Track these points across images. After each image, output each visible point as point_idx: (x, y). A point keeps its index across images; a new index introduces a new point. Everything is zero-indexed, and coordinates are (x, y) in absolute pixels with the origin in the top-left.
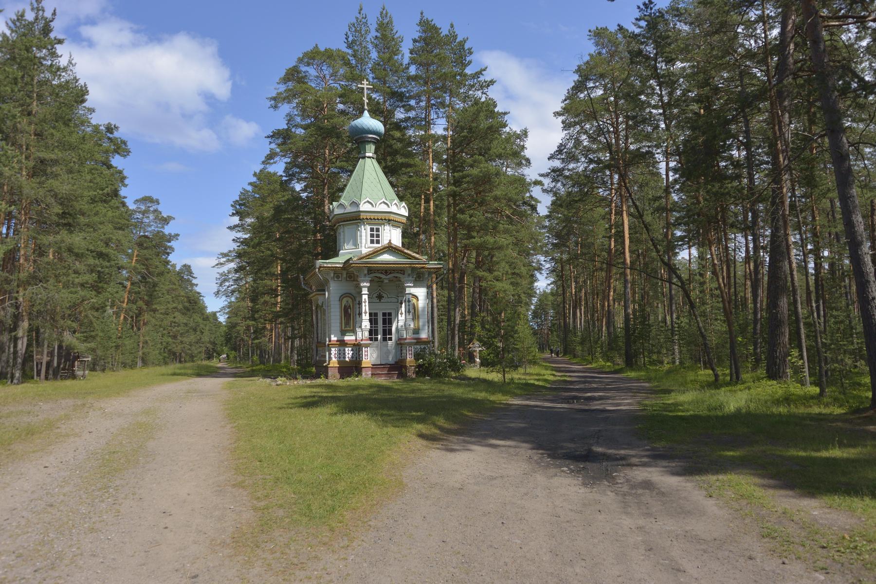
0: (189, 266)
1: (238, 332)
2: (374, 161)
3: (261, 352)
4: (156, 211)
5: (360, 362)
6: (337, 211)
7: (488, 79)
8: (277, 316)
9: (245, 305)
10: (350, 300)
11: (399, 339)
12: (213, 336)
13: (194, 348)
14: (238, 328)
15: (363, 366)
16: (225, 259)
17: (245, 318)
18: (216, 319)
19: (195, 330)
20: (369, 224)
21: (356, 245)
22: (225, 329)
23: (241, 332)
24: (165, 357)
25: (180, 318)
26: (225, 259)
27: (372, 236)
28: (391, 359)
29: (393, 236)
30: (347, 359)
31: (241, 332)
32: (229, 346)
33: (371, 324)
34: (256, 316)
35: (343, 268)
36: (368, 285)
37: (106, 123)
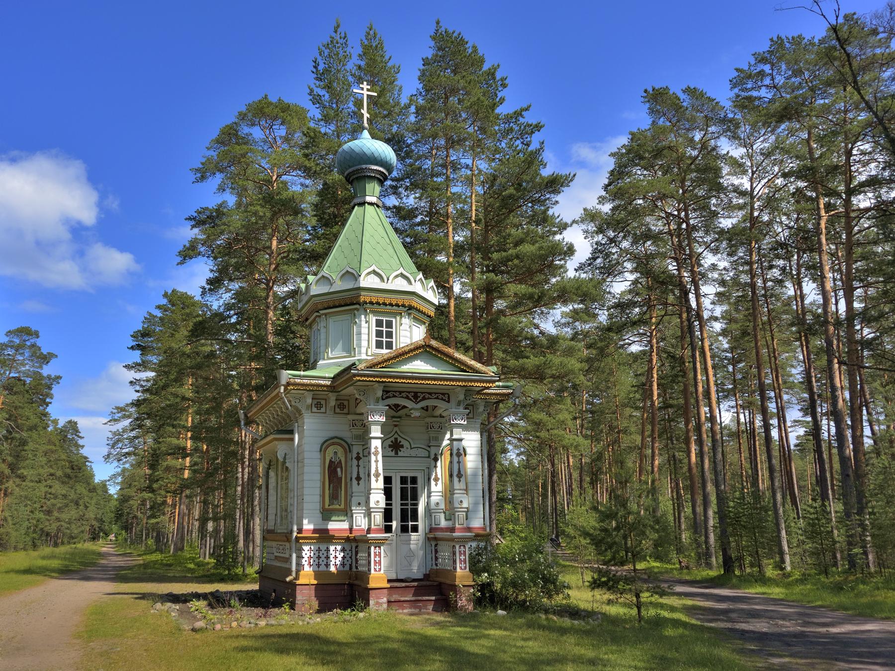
0: (76, 423)
1: (131, 508)
3: (158, 535)
4: (33, 345)
5: (364, 576)
6: (315, 290)
8: (185, 485)
9: (142, 473)
10: (340, 451)
11: (432, 530)
12: (101, 512)
13: (73, 526)
14: (131, 502)
15: (372, 585)
16: (120, 415)
17: (142, 490)
18: (105, 490)
19: (77, 504)
20: (374, 313)
21: (349, 349)
22: (116, 503)
23: (135, 507)
24: (34, 538)
25: (58, 488)
27: (379, 334)
28: (416, 570)
30: (333, 569)
31: (135, 507)
32: (119, 523)
34: (155, 486)
35: (332, 388)
36: (383, 419)
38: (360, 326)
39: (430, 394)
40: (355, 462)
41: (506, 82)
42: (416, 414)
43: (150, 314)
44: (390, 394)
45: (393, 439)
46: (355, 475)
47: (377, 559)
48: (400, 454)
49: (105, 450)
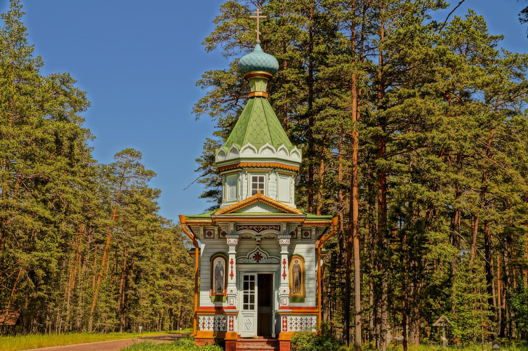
2: (266, 102)
10: (222, 261)
20: (251, 173)
27: (254, 186)
38: (242, 182)
39: (268, 226)
41: (94, 139)
44: (242, 227)
45: (256, 253)
47: (285, 324)
48: (260, 262)
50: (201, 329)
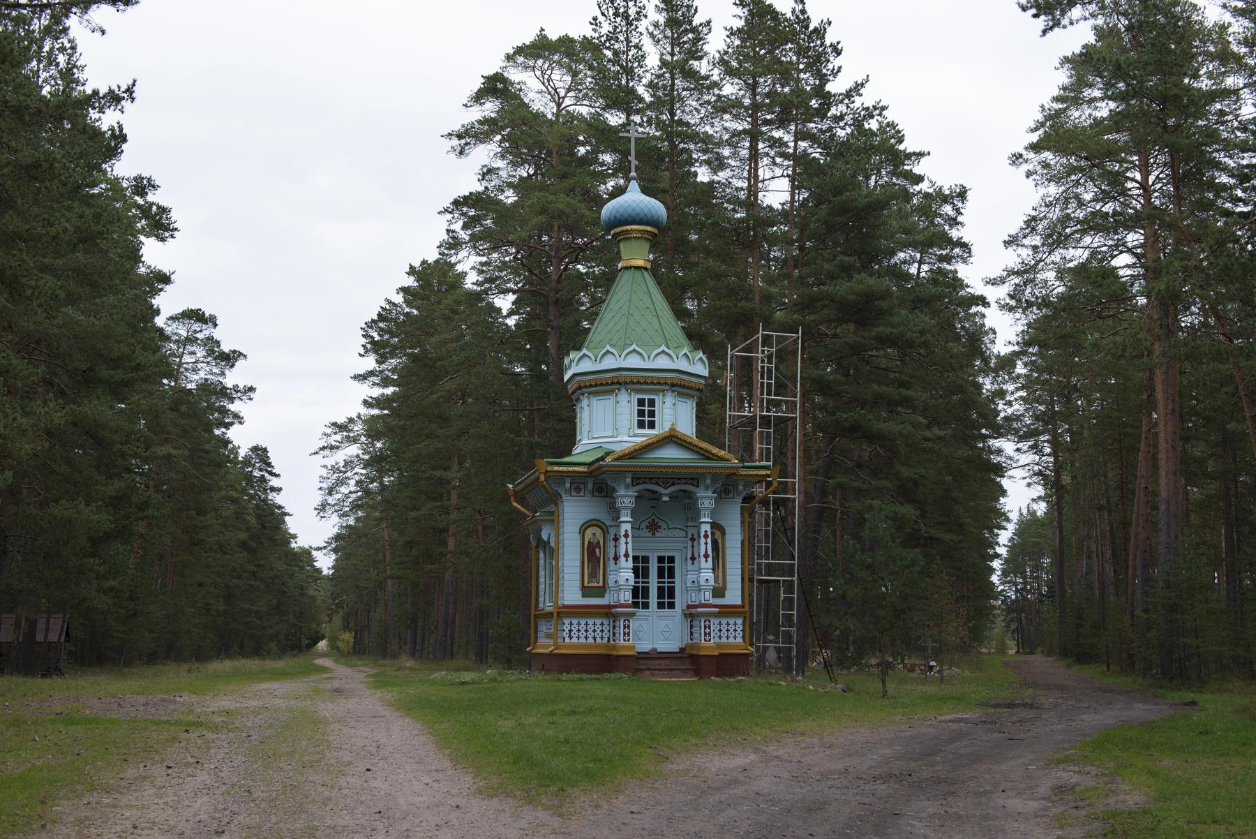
7: (869, 103)
10: (598, 532)
16: (338, 437)
18: (311, 560)
20: (638, 391)
26: (338, 437)
27: (641, 413)
29: (677, 415)
33: (637, 576)
37: (133, 175)
40: (613, 543)
42: (666, 499)
43: (389, 302)
46: (612, 555)
49: (318, 498)
50: (567, 640)
